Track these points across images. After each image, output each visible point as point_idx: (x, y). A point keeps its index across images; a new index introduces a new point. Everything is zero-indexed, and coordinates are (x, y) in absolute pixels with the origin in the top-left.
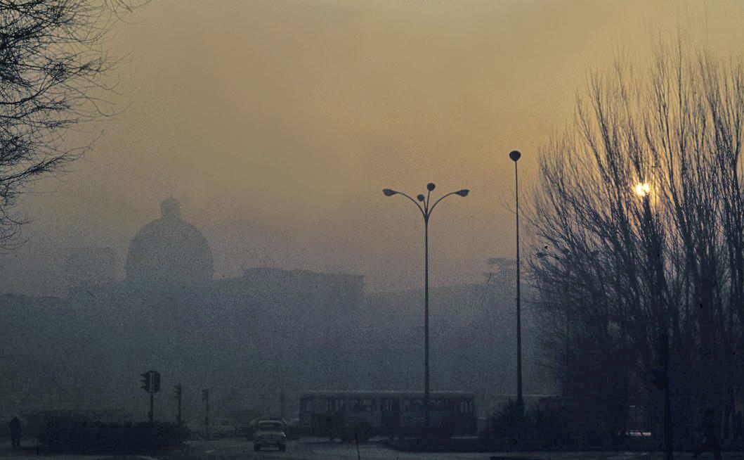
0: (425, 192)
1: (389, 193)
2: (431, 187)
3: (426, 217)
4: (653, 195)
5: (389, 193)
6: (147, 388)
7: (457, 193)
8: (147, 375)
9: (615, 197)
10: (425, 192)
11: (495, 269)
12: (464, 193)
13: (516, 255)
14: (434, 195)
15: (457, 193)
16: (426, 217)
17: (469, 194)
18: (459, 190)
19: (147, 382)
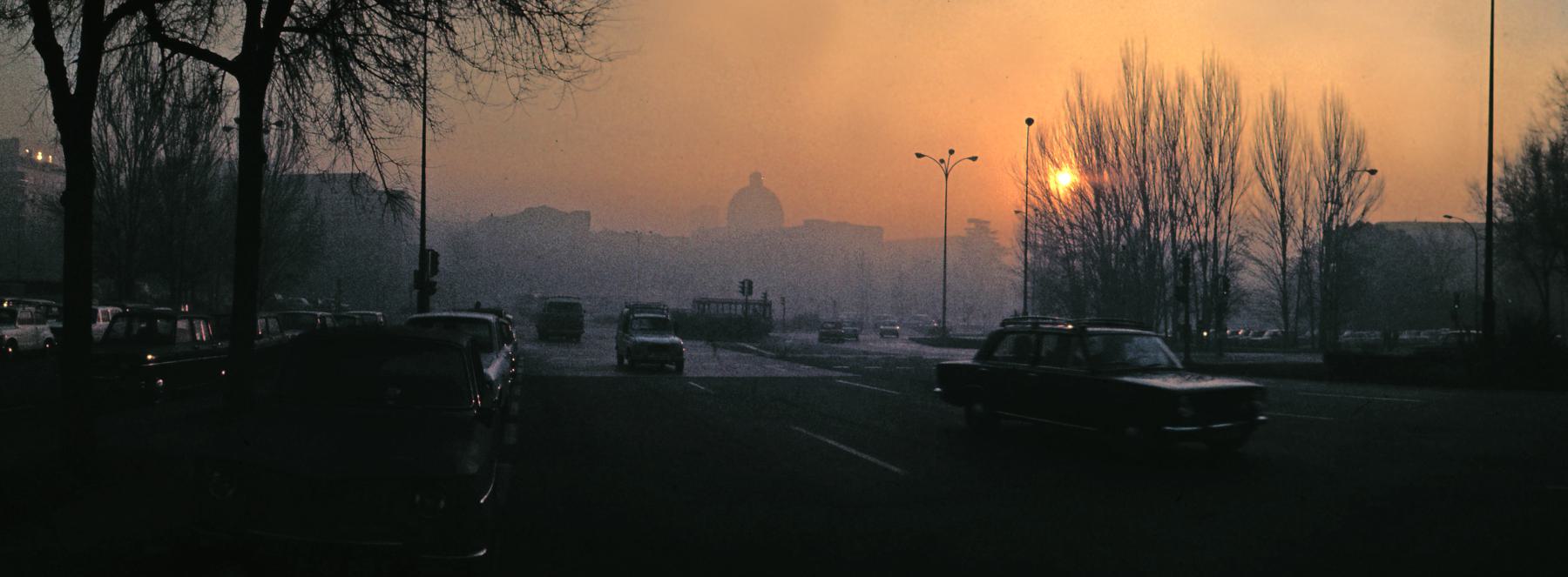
0: (946, 157)
1: (919, 156)
2: (952, 152)
3: (947, 175)
4: (1527, 169)
5: (919, 156)
6: (743, 292)
7: (970, 158)
8: (743, 283)
9: (1325, 180)
10: (946, 157)
11: (972, 226)
12: (974, 159)
13: (943, 260)
14: (955, 157)
15: (970, 158)
16: (947, 175)
17: (1377, 174)
18: (971, 156)
19: (743, 288)
